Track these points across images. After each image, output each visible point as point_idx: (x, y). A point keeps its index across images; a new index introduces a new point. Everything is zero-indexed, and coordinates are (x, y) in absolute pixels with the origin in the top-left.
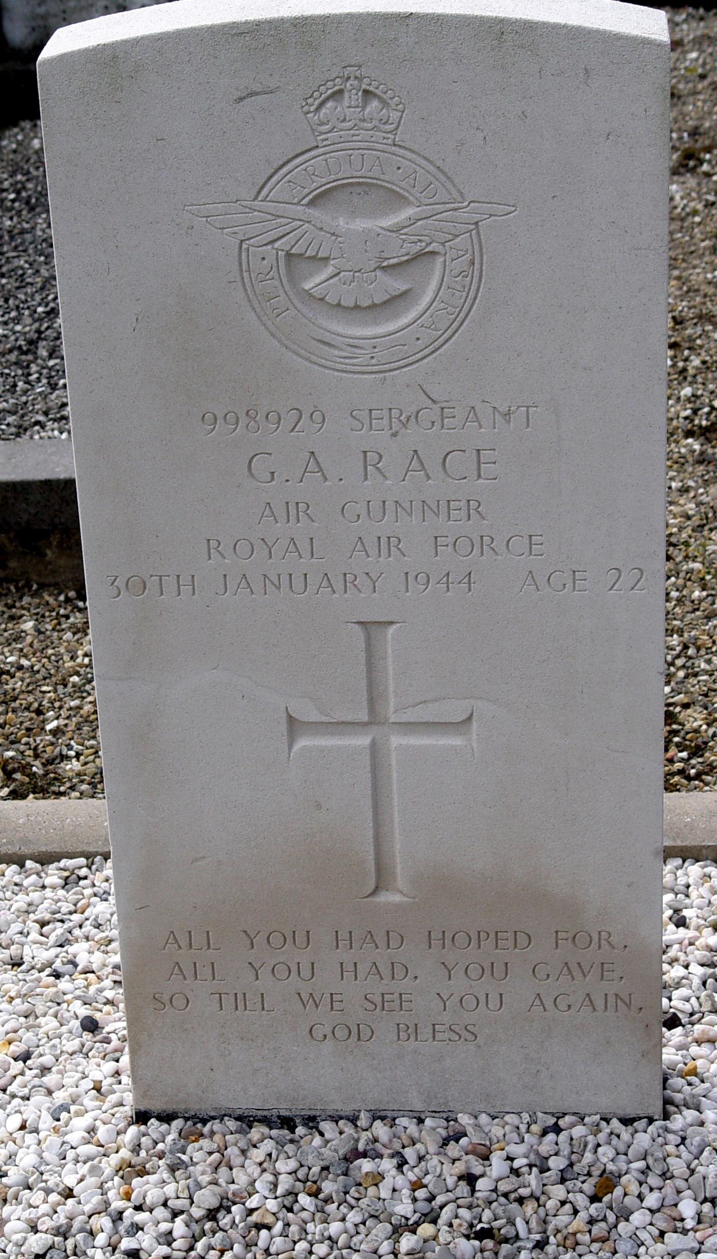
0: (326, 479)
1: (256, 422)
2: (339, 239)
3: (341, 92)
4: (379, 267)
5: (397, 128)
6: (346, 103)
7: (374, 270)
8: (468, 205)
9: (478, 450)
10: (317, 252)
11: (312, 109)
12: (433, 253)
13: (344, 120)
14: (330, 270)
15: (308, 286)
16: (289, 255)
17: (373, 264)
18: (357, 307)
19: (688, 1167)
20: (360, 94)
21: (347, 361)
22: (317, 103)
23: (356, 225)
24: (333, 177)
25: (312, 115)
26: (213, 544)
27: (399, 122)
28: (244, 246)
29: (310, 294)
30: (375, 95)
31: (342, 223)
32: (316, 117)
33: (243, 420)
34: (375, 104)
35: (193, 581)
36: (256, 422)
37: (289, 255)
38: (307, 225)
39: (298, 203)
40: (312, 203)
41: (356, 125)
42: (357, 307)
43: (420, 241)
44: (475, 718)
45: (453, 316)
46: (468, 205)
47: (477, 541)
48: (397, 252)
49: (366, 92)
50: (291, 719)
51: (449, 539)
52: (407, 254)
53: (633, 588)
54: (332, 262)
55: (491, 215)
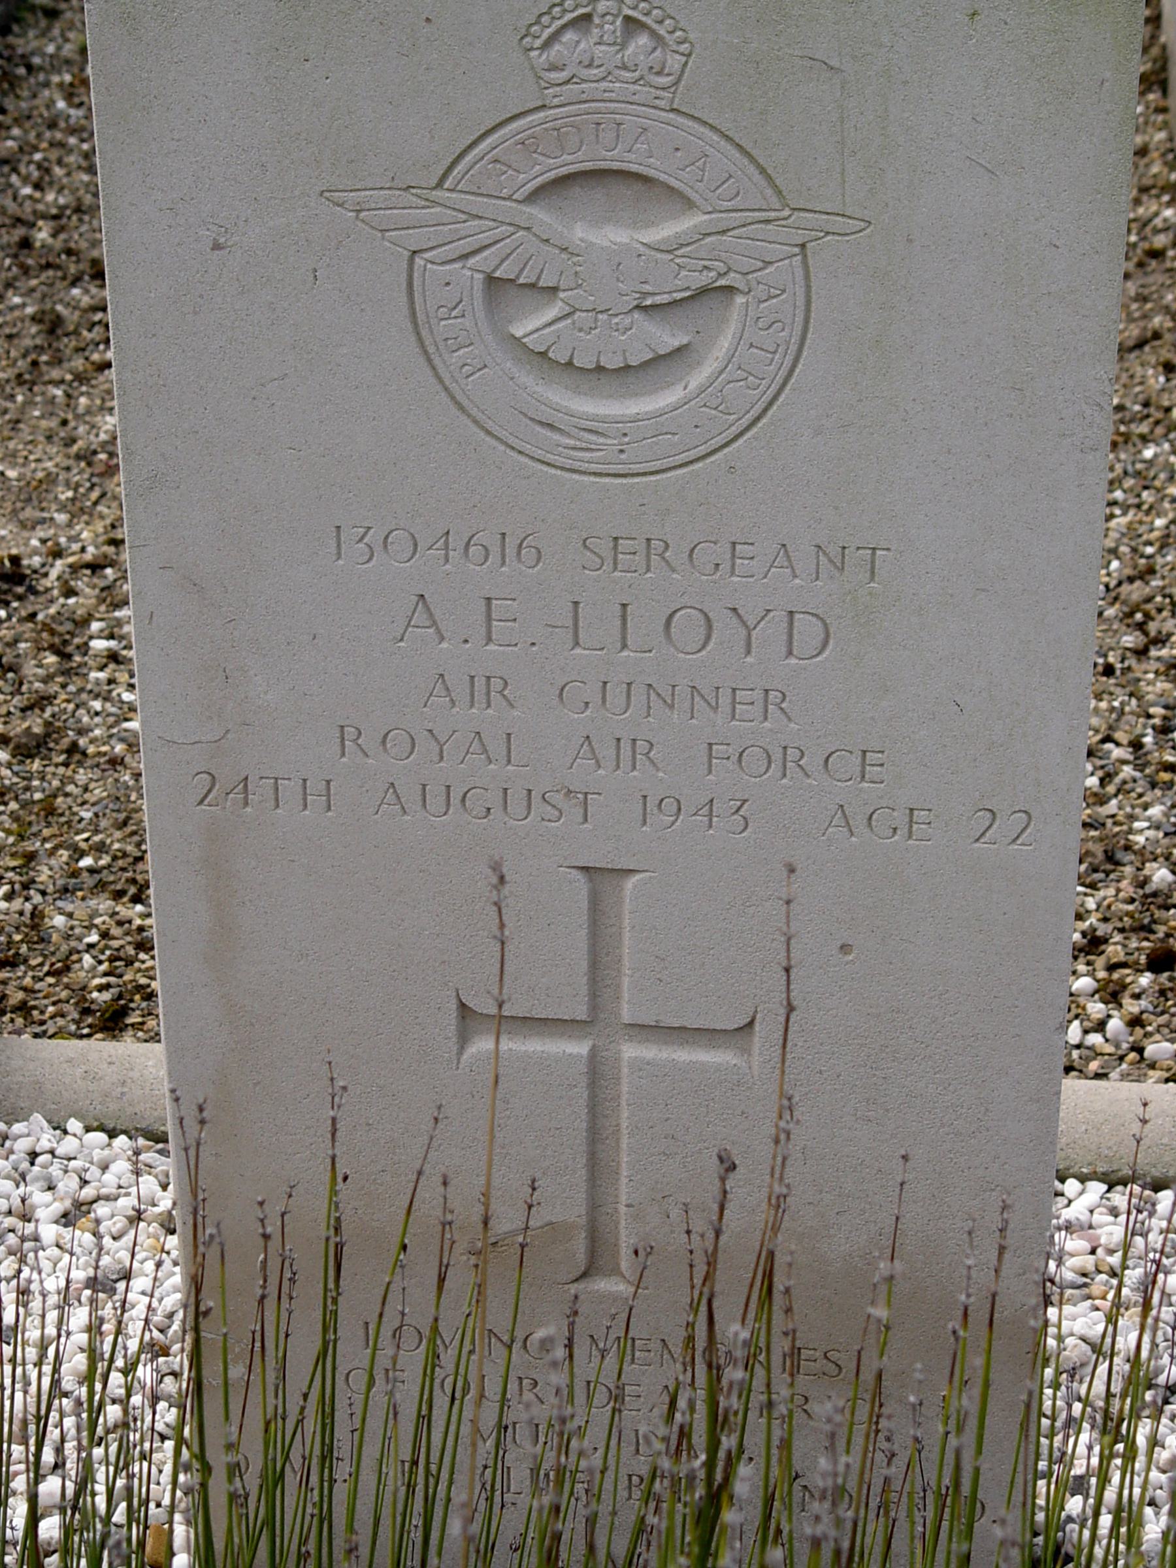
0: (442, 639)
2: (576, 259)
3: (587, 17)
4: (637, 307)
5: (676, 83)
8: (790, 216)
9: (489, 599)
10: (539, 278)
11: (538, 43)
12: (730, 290)
13: (589, 66)
16: (491, 281)
22: (547, 33)
23: (604, 235)
25: (536, 53)
27: (683, 72)
28: (419, 261)
29: (524, 344)
31: (580, 233)
32: (544, 57)
34: (643, 40)
35: (328, 789)
37: (491, 281)
39: (509, 198)
40: (533, 197)
41: (642, 78)
43: (706, 267)
44: (757, 1027)
46: (790, 216)
47: (777, 755)
49: (628, 19)
50: (462, 1006)
52: (688, 288)
53: (977, 840)
55: (828, 233)
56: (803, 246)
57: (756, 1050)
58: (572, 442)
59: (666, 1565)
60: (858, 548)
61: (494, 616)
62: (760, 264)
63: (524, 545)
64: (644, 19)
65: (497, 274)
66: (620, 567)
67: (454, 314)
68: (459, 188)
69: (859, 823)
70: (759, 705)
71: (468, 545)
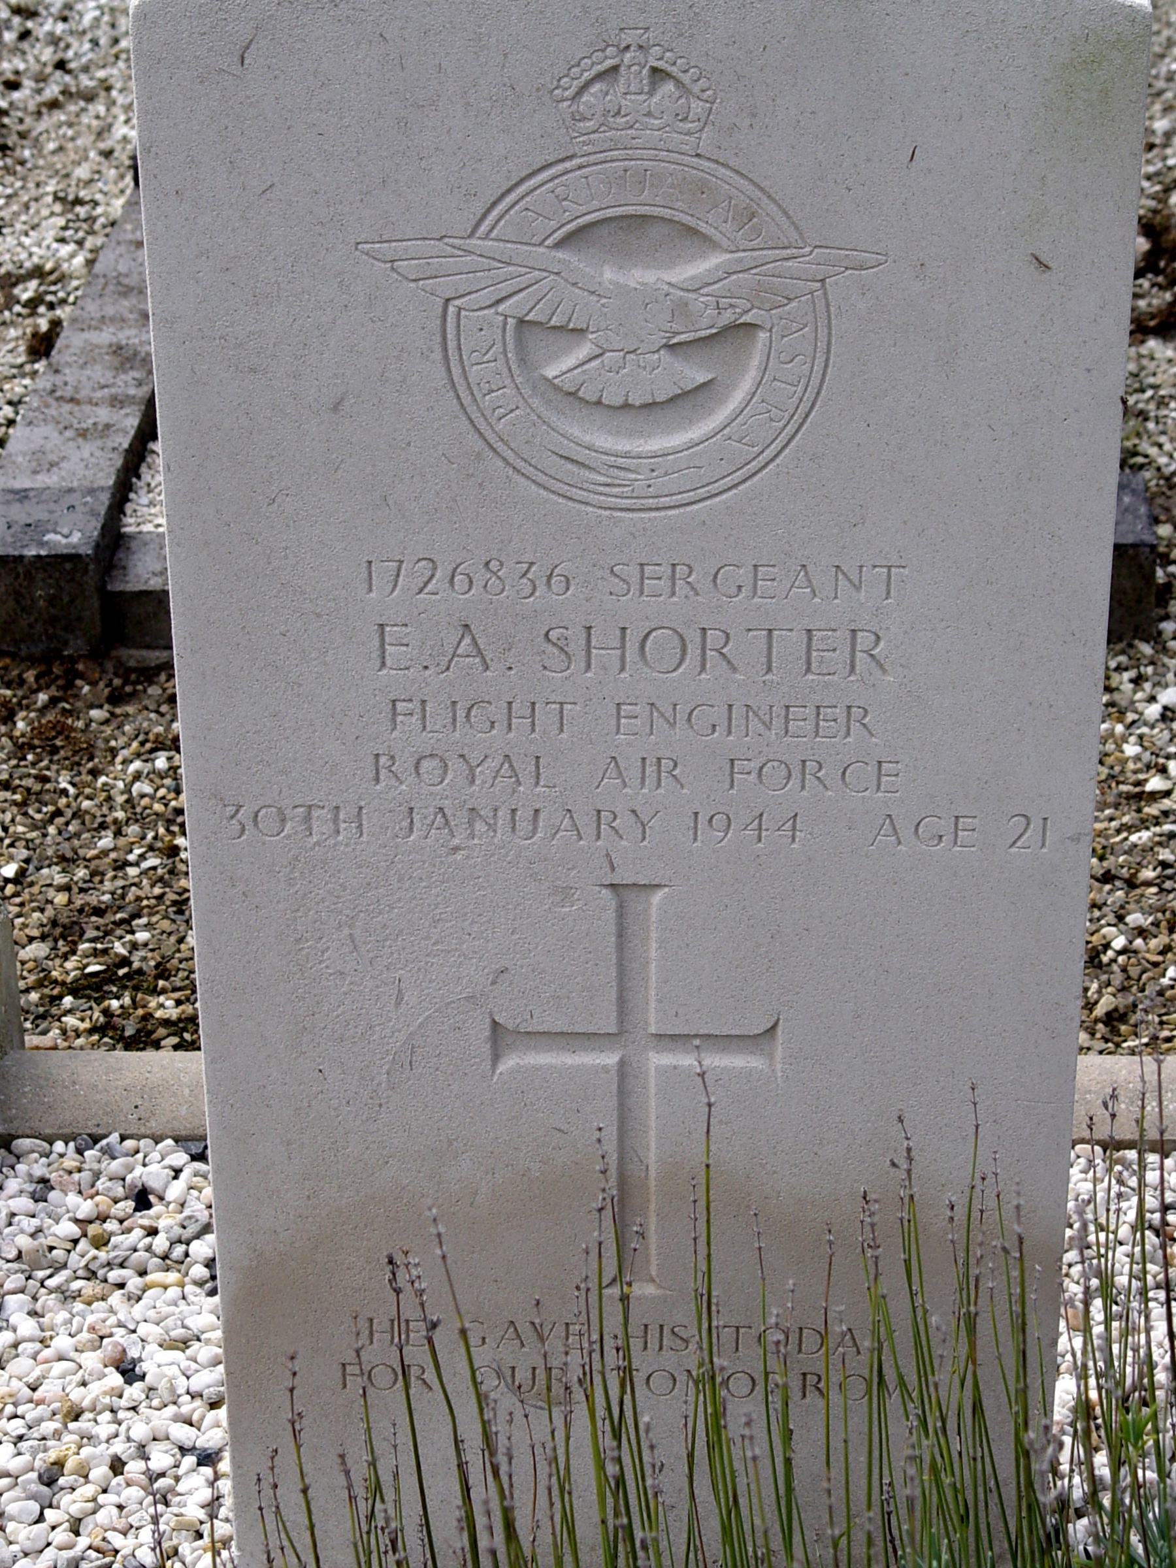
1: (499, 578)
2: (603, 301)
3: (615, 68)
4: (666, 346)
6: (621, 88)
7: (658, 351)
8: (812, 252)
14: (584, 350)
15: (551, 372)
16: (521, 322)
17: (659, 340)
18: (626, 406)
19: (63, 1390)
20: (645, 71)
21: (606, 490)
24: (596, 204)
26: (383, 760)
28: (451, 309)
30: (669, 75)
33: (480, 577)
34: (669, 87)
36: (499, 578)
37: (521, 322)
38: (552, 277)
40: (558, 245)
42: (626, 406)
43: (731, 306)
45: (781, 424)
46: (812, 252)
48: (707, 321)
49: (655, 70)
50: (495, 1023)
51: (752, 764)
54: (591, 336)
55: (847, 268)
56: (823, 281)
57: (779, 1053)
58: (602, 479)
59: (869, 1565)
60: (875, 567)
61: (593, 644)
62: (786, 301)
63: (556, 571)
64: (669, 69)
65: (527, 318)
66: (759, 593)
67: (485, 358)
68: (493, 235)
69: (906, 833)
70: (842, 720)
71: (453, 577)
